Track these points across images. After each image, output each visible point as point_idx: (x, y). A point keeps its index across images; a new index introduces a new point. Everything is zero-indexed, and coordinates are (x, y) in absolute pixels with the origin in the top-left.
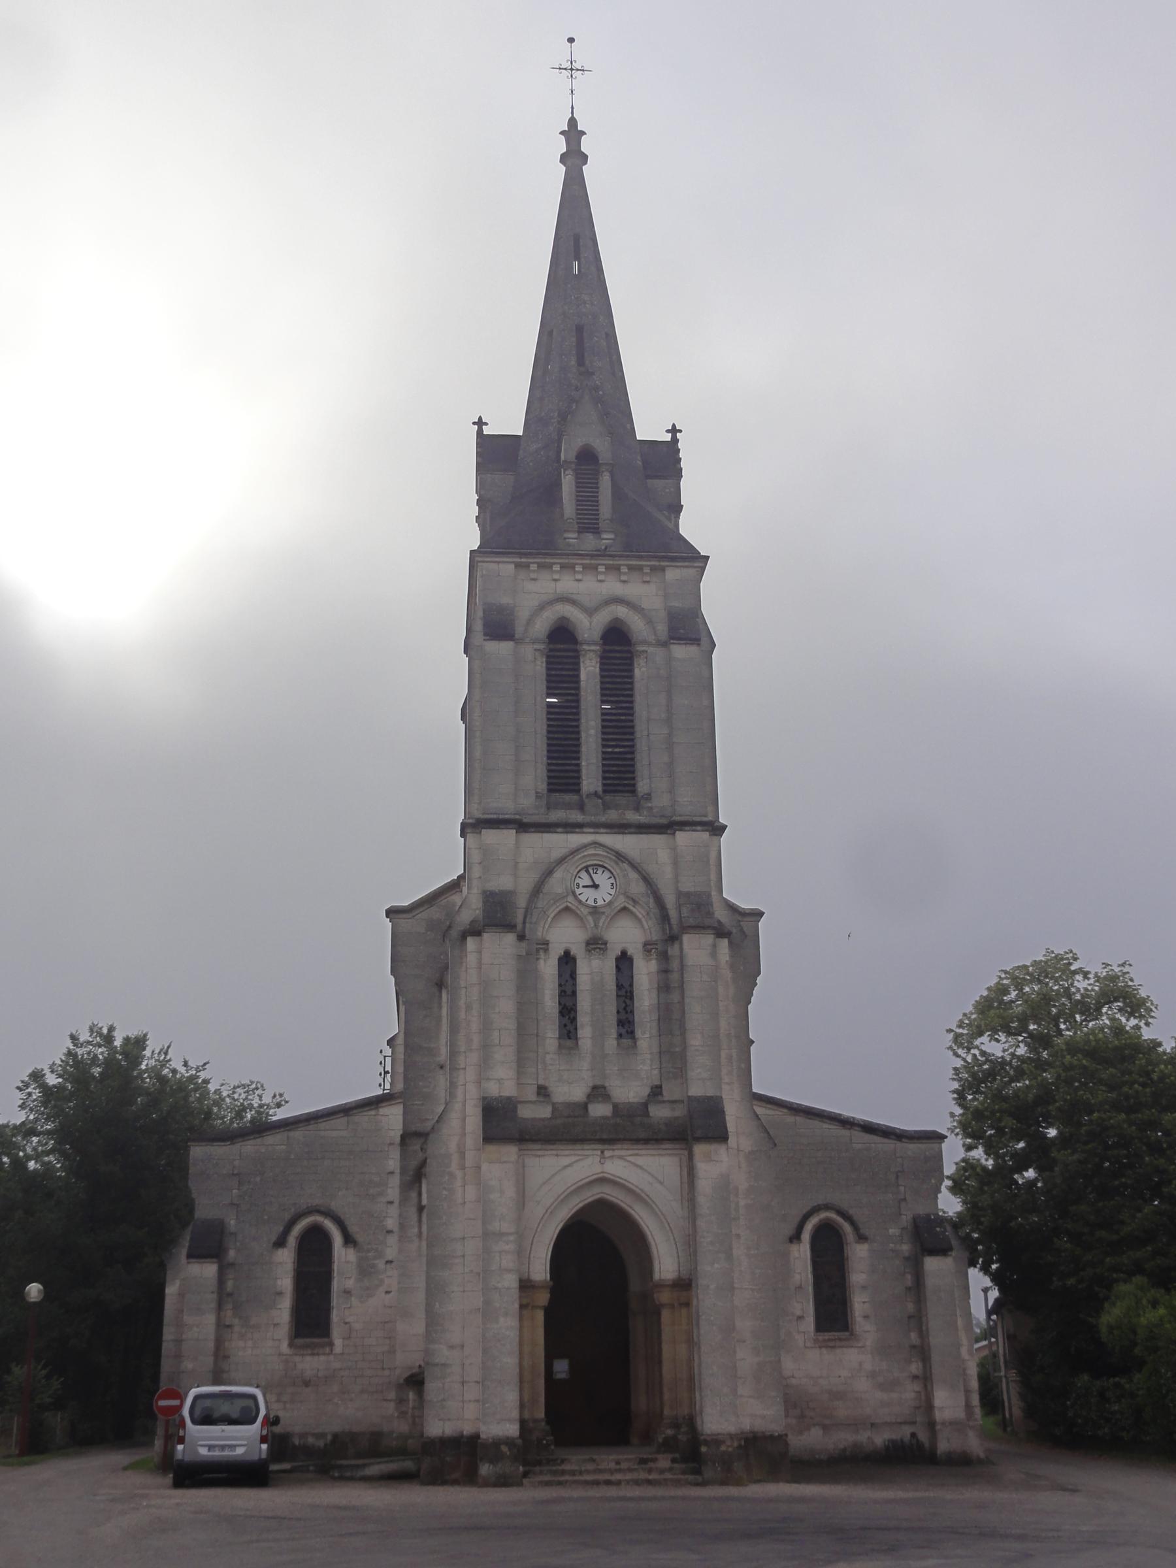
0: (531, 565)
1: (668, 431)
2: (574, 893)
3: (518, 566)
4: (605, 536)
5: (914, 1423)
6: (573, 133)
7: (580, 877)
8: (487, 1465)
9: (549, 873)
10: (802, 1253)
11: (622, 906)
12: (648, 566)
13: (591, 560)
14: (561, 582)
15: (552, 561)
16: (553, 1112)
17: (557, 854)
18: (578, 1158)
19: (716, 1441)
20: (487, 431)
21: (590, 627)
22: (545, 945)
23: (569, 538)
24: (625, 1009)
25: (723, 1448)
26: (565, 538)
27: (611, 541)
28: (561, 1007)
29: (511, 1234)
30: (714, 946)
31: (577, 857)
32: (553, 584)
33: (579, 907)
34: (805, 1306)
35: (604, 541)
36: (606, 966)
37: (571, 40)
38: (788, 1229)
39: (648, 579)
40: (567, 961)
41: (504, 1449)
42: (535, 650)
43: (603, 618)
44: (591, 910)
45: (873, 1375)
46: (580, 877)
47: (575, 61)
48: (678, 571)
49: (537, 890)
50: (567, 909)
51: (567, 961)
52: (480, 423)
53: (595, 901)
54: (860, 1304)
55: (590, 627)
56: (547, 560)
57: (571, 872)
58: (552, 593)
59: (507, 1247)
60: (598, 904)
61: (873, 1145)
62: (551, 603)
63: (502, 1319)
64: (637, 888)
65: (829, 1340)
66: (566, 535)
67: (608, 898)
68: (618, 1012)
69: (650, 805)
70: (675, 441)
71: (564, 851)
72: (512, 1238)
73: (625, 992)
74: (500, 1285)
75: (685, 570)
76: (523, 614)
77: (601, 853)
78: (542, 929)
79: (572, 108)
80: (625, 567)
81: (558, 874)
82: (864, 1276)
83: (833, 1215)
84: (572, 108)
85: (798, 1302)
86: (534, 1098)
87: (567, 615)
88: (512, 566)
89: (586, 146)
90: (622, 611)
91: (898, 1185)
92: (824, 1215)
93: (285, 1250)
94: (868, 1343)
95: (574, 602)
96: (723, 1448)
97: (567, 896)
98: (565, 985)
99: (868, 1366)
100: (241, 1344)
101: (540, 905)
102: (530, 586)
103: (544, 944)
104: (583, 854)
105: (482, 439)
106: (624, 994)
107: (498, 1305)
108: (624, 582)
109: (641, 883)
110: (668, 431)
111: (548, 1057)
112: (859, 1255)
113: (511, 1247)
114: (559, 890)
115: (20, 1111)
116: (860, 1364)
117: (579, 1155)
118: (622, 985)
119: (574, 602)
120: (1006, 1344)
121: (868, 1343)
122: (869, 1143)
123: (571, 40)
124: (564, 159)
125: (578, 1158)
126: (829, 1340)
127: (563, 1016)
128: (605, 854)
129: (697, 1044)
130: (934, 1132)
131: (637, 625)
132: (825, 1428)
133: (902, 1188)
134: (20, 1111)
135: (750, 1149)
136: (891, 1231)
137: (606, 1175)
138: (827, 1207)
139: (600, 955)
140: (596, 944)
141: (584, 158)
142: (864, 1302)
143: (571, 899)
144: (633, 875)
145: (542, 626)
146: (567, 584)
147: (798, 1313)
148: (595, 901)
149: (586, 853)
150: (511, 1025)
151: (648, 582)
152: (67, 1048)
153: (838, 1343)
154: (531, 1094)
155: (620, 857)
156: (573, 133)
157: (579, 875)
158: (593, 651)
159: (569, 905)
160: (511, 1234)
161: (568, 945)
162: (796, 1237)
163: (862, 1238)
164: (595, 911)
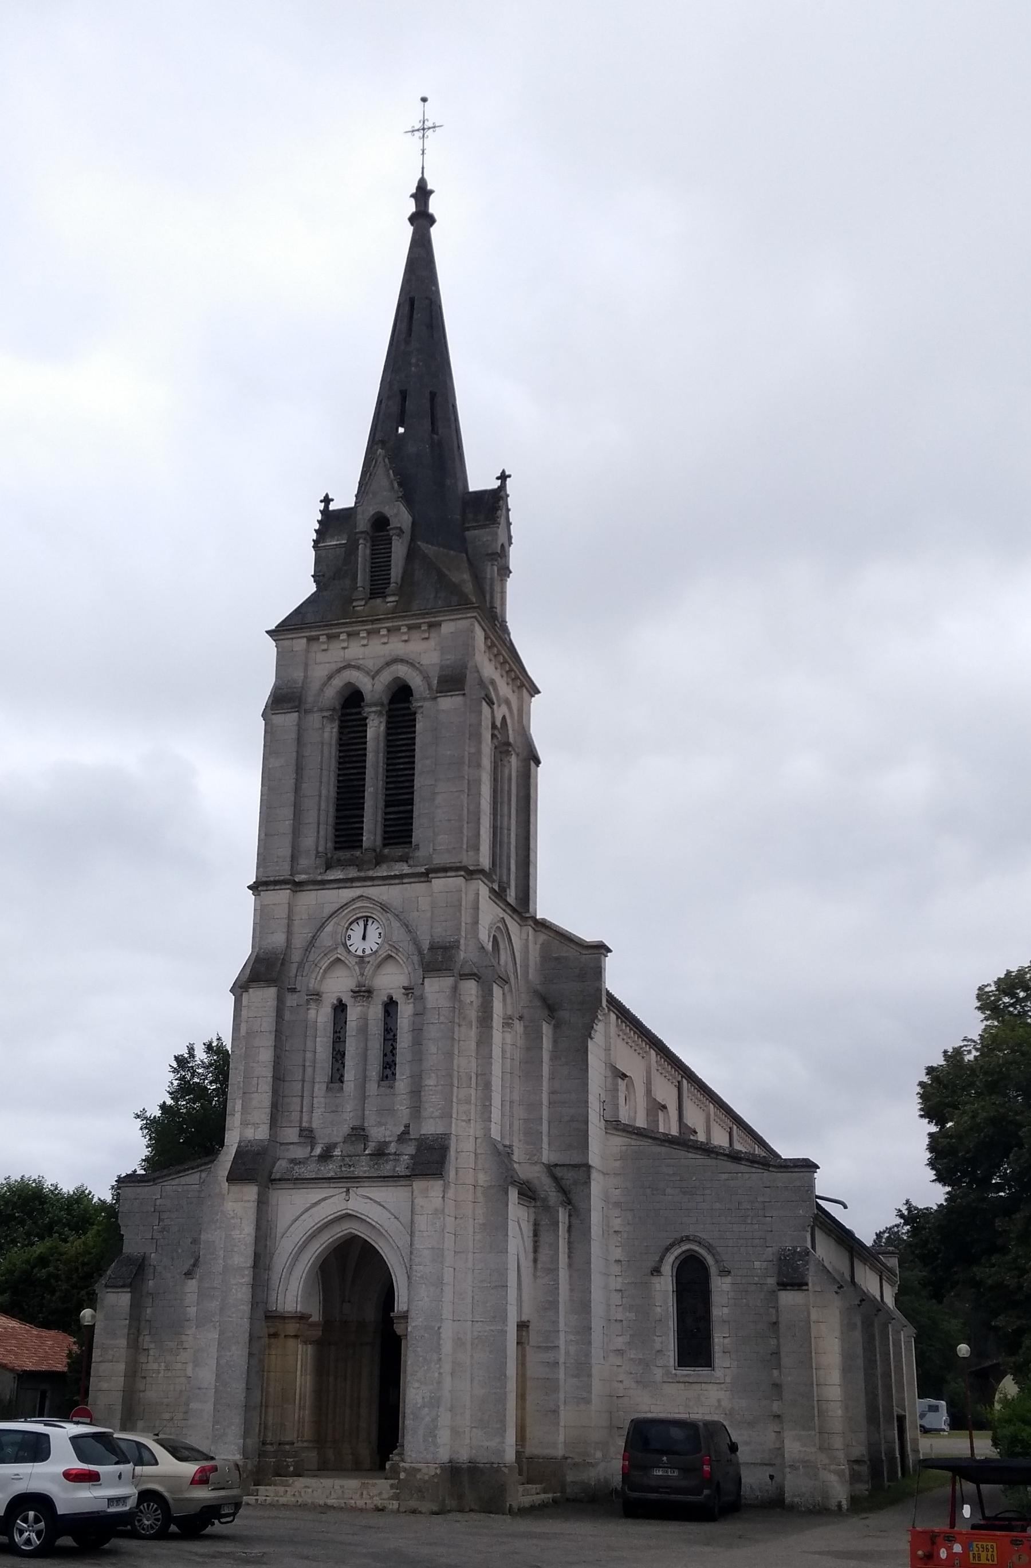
0: (321, 637)
1: (498, 478)
2: (345, 945)
3: (311, 639)
4: (389, 599)
5: (772, 1465)
6: (422, 194)
7: (351, 929)
9: (322, 926)
10: (665, 1285)
12: (424, 623)
13: (372, 624)
14: (350, 649)
15: (337, 631)
17: (328, 910)
20: (332, 507)
21: (373, 688)
22: (316, 996)
23: (358, 606)
24: (391, 1052)
26: (354, 607)
28: (335, 1053)
31: (346, 911)
32: (342, 653)
33: (348, 957)
34: (668, 1341)
35: (388, 604)
36: (375, 1011)
37: (424, 100)
38: (650, 1264)
39: (426, 635)
40: (340, 1008)
42: (323, 717)
43: (386, 677)
46: (351, 929)
47: (428, 120)
48: (452, 624)
49: (312, 943)
50: (338, 960)
51: (340, 1008)
52: (327, 500)
53: (364, 951)
54: (720, 1339)
55: (373, 688)
56: (334, 631)
57: (343, 925)
58: (341, 661)
60: (366, 953)
62: (339, 670)
64: (399, 934)
67: (375, 947)
68: (385, 1055)
70: (502, 487)
71: (337, 906)
73: (390, 1034)
75: (460, 622)
76: (314, 686)
77: (368, 905)
78: (314, 980)
79: (423, 168)
80: (405, 627)
82: (726, 1310)
84: (423, 168)
86: (296, 1140)
87: (401, 674)
89: (434, 206)
90: (402, 671)
93: (194, 1280)
95: (357, 668)
97: (336, 948)
98: (340, 1032)
100: (155, 1366)
101: (311, 958)
102: (320, 657)
103: (317, 995)
104: (351, 908)
105: (325, 512)
106: (392, 1037)
108: (406, 641)
109: (403, 930)
110: (498, 478)
112: (721, 1288)
116: (719, 1401)
118: (391, 1029)
119: (357, 668)
122: (737, 1173)
123: (424, 100)
124: (412, 219)
127: (337, 1061)
128: (372, 906)
129: (432, 1084)
130: (807, 1160)
131: (416, 682)
137: (349, 1211)
138: (687, 1239)
139: (363, 1002)
140: (362, 993)
141: (431, 220)
143: (341, 950)
144: (396, 924)
145: (331, 693)
146: (355, 650)
147: (658, 1346)
148: (364, 951)
149: (354, 907)
150: (269, 1073)
151: (426, 639)
152: (917, 1094)
154: (291, 1134)
155: (385, 908)
156: (422, 194)
157: (351, 927)
158: (374, 712)
159: (339, 956)
161: (391, 991)
163: (725, 1272)
164: (362, 960)
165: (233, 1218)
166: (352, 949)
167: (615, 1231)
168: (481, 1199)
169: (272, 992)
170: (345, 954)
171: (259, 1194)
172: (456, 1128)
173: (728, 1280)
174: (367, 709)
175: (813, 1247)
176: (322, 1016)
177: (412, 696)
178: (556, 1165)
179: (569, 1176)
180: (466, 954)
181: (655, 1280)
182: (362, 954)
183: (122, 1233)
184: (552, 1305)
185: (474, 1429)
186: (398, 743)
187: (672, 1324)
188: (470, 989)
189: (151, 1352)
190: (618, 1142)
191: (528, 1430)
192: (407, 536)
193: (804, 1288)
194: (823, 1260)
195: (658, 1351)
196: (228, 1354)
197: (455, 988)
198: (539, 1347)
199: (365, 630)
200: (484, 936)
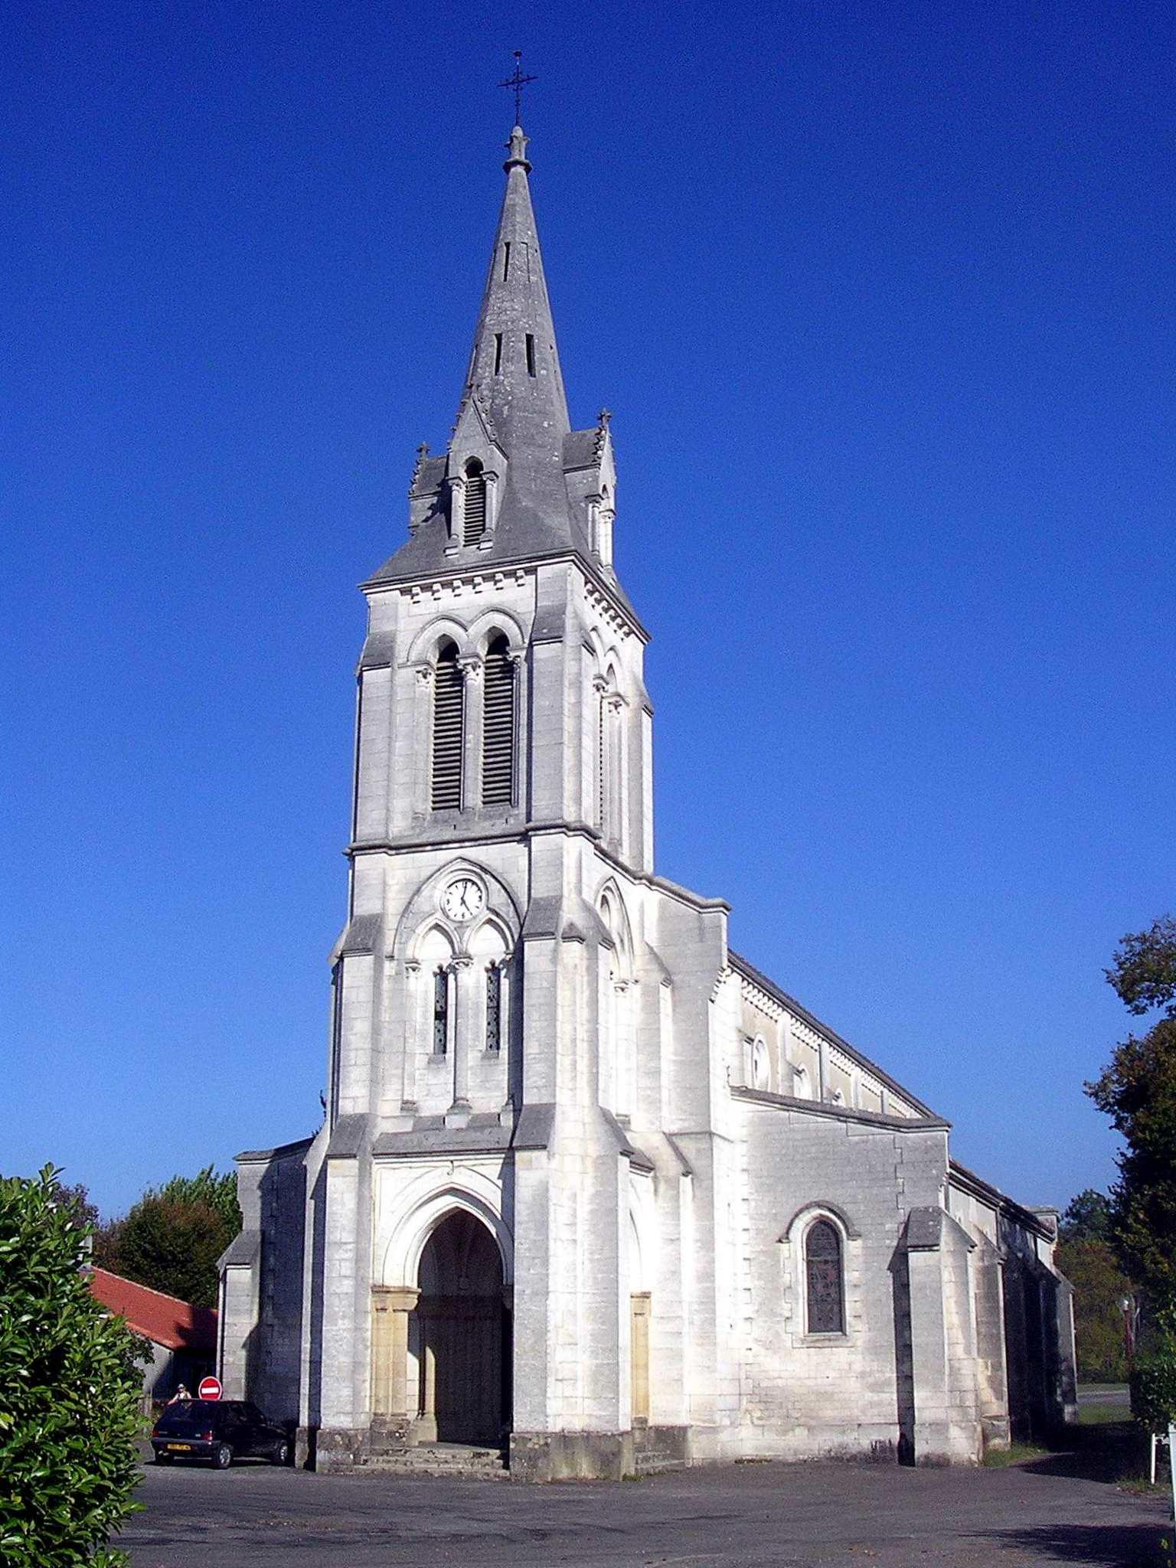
4: (483, 546)
8: (323, 1452)
9: (418, 891)
10: (796, 1251)
11: (487, 918)
16: (414, 1125)
18: (427, 1170)
19: (524, 1439)
21: (473, 642)
25: (530, 1445)
27: (489, 550)
29: (350, 1243)
30: (555, 951)
38: (780, 1230)
41: (338, 1438)
44: (456, 925)
45: (862, 1375)
55: (473, 642)
59: (346, 1256)
61: (871, 1137)
62: (431, 622)
63: (340, 1322)
65: (817, 1340)
66: (448, 552)
69: (517, 812)
72: (350, 1247)
74: (337, 1291)
81: (426, 891)
82: (856, 1274)
83: (817, 1212)
85: (786, 1303)
88: (398, 592)
90: (499, 620)
91: (896, 1178)
92: (817, 1212)
94: (859, 1343)
96: (530, 1445)
99: (858, 1367)
100: (280, 1341)
103: (416, 963)
104: (450, 870)
107: (337, 1309)
111: (417, 1072)
113: (350, 1255)
114: (427, 908)
115: (1096, 1110)
117: (429, 1167)
120: (306, 1356)
121: (859, 1343)
122: (867, 1135)
125: (427, 1170)
126: (817, 1340)
132: (810, 1429)
133: (900, 1181)
134: (1096, 1110)
135: (598, 1154)
136: (888, 1227)
142: (856, 1301)
147: (788, 1314)
153: (827, 1343)
160: (350, 1243)
162: (784, 1238)
165: (335, 1193)
166: (451, 914)
167: (575, 1195)
168: (590, 1169)
169: (369, 959)
170: (444, 919)
171: (360, 1169)
172: (563, 1098)
173: (859, 1242)
174: (462, 662)
175: (947, 1207)
176: (423, 986)
177: (509, 645)
178: (675, 1135)
179: (688, 1147)
180: (570, 913)
181: (784, 1247)
182: (461, 919)
183: (241, 1210)
184: (675, 1273)
185: (586, 1400)
186: (448, 677)
187: (802, 1289)
188: (573, 951)
189: (276, 1328)
190: (746, 1110)
191: (651, 1400)
192: (502, 478)
193: (936, 1248)
194: (960, 1219)
195: (788, 1318)
196: (334, 1328)
197: (555, 951)
198: (662, 1318)
199: (459, 579)
200: (588, 895)
